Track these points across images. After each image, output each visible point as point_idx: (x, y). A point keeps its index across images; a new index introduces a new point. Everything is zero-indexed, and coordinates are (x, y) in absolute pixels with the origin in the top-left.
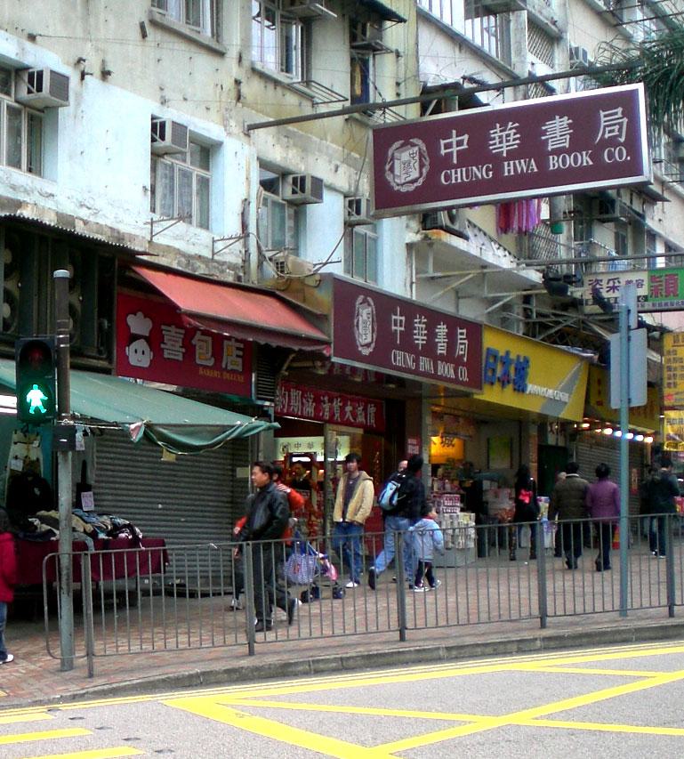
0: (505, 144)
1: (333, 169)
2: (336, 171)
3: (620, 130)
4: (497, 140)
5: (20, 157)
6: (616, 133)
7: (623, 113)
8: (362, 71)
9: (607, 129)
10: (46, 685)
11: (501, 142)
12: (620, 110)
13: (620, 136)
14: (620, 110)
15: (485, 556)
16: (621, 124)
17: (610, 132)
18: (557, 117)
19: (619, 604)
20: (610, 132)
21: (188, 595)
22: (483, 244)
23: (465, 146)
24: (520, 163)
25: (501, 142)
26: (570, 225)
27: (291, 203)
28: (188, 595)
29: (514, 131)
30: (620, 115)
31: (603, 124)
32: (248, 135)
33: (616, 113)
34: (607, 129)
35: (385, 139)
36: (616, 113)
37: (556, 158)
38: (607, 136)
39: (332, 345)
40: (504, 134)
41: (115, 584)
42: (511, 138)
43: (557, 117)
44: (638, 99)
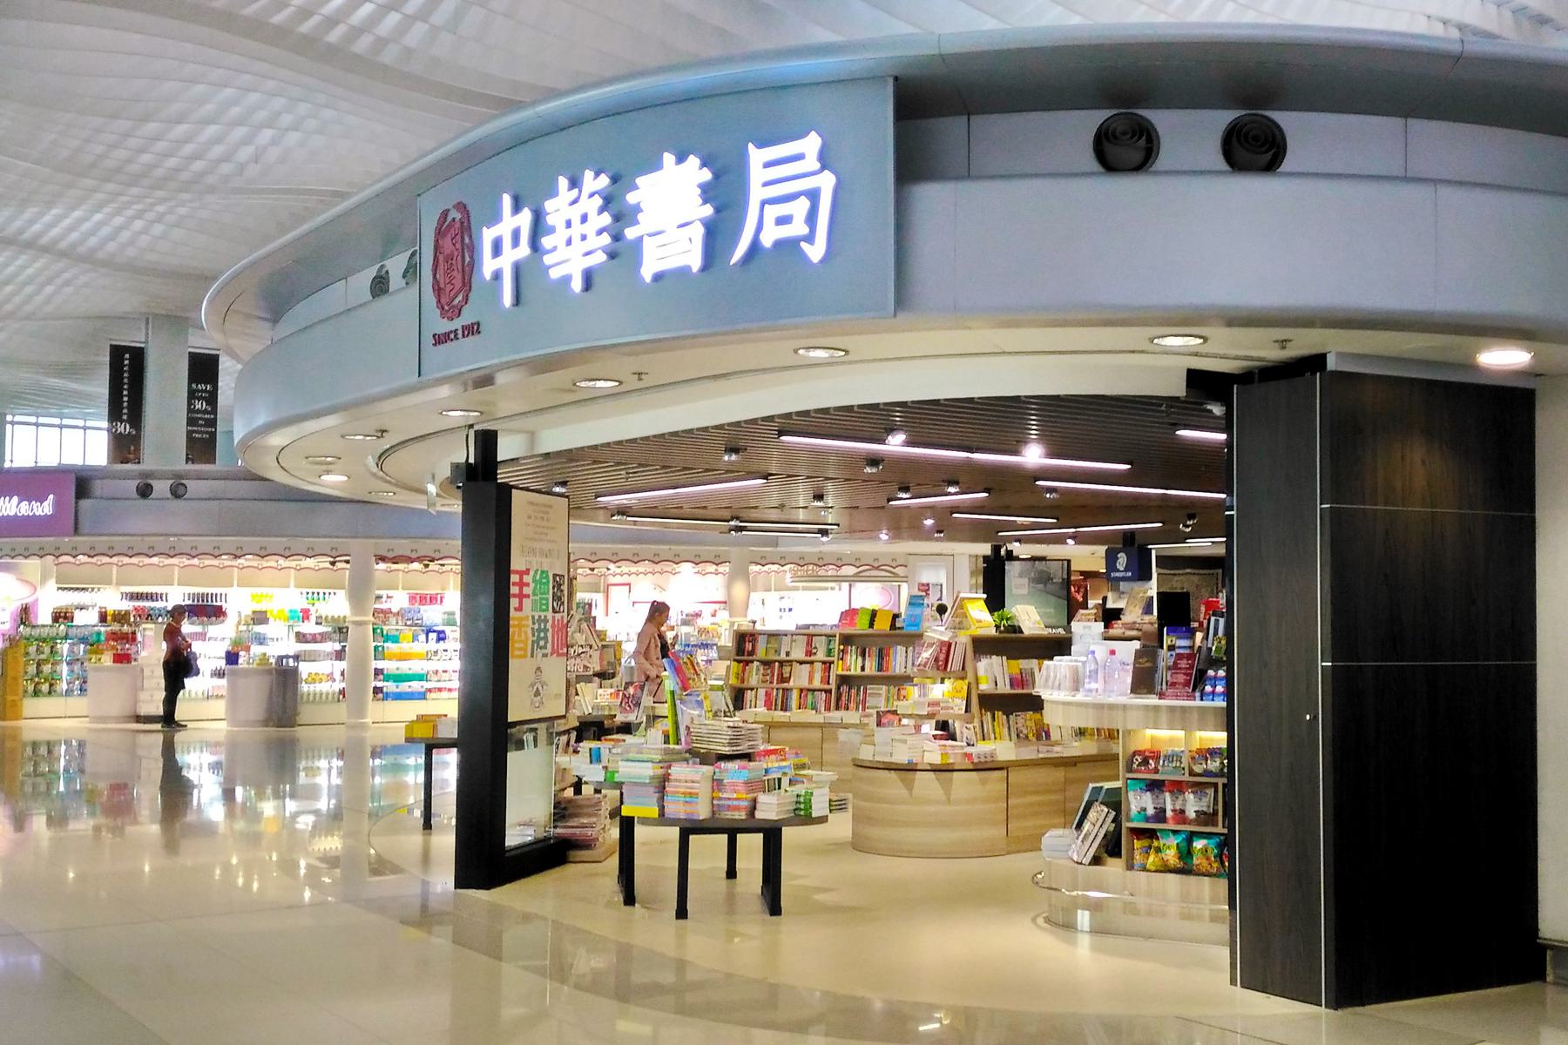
2: (391, 597)
3: (811, 218)
5: (248, 536)
6: (798, 228)
8: (1230, 580)
12: (811, 144)
13: (810, 238)
14: (811, 144)
16: (813, 195)
17: (783, 221)
19: (1186, 641)
20: (783, 221)
24: (500, 474)
26: (1082, 926)
27: (824, 663)
30: (812, 163)
31: (757, 193)
33: (800, 157)
34: (772, 212)
36: (800, 157)
37: (119, 424)
38: (767, 240)
41: (1173, 909)
44: (1098, 468)
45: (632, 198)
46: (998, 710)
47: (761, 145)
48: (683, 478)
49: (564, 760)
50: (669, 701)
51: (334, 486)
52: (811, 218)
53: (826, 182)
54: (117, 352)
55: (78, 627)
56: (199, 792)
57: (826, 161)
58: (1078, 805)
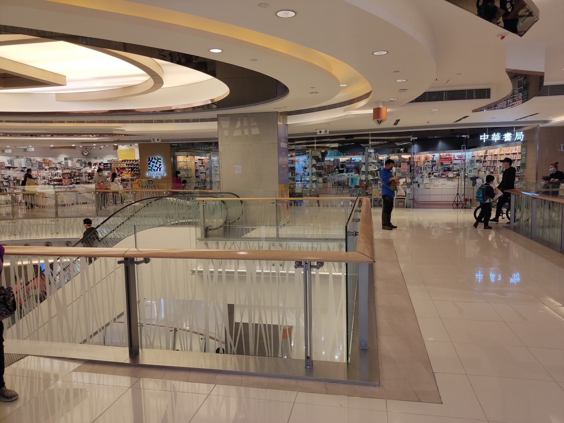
0: (496, 138)
1: (144, 217)
3: (521, 138)
4: (494, 137)
6: (520, 138)
7: (522, 133)
9: (518, 137)
10: (284, 222)
11: (495, 138)
13: (521, 139)
15: (226, 274)
16: (522, 136)
18: (494, 133)
21: (325, 206)
22: (87, 392)
23: (481, 136)
25: (495, 138)
28: (325, 206)
29: (499, 135)
30: (521, 134)
32: (185, 182)
34: (518, 137)
35: (421, 173)
39: (224, 250)
40: (496, 136)
42: (498, 137)
43: (494, 133)
44: (133, 254)
45: (504, 135)
46: (481, 209)
47: (517, 132)
48: (92, 230)
49: (115, 158)
50: (71, 190)
51: (51, 259)
52: (521, 138)
53: (523, 135)
54: (489, 90)
55: (500, 223)
56: (528, 6)
57: (523, 134)
58: (219, 197)
